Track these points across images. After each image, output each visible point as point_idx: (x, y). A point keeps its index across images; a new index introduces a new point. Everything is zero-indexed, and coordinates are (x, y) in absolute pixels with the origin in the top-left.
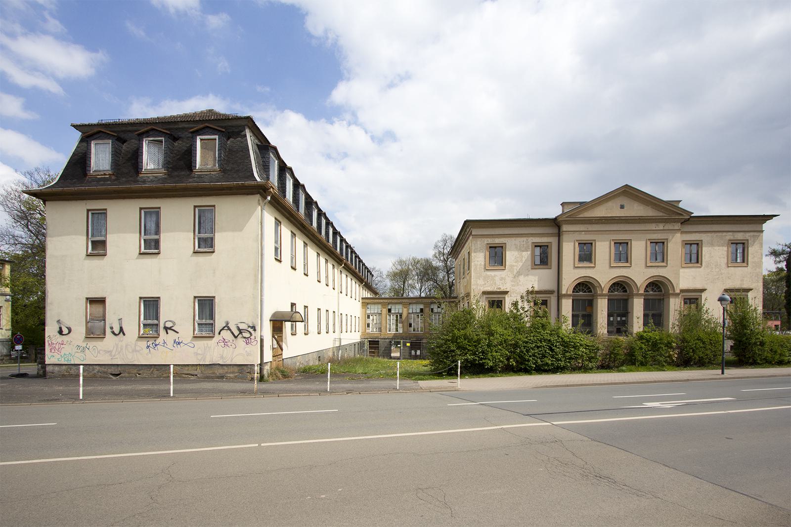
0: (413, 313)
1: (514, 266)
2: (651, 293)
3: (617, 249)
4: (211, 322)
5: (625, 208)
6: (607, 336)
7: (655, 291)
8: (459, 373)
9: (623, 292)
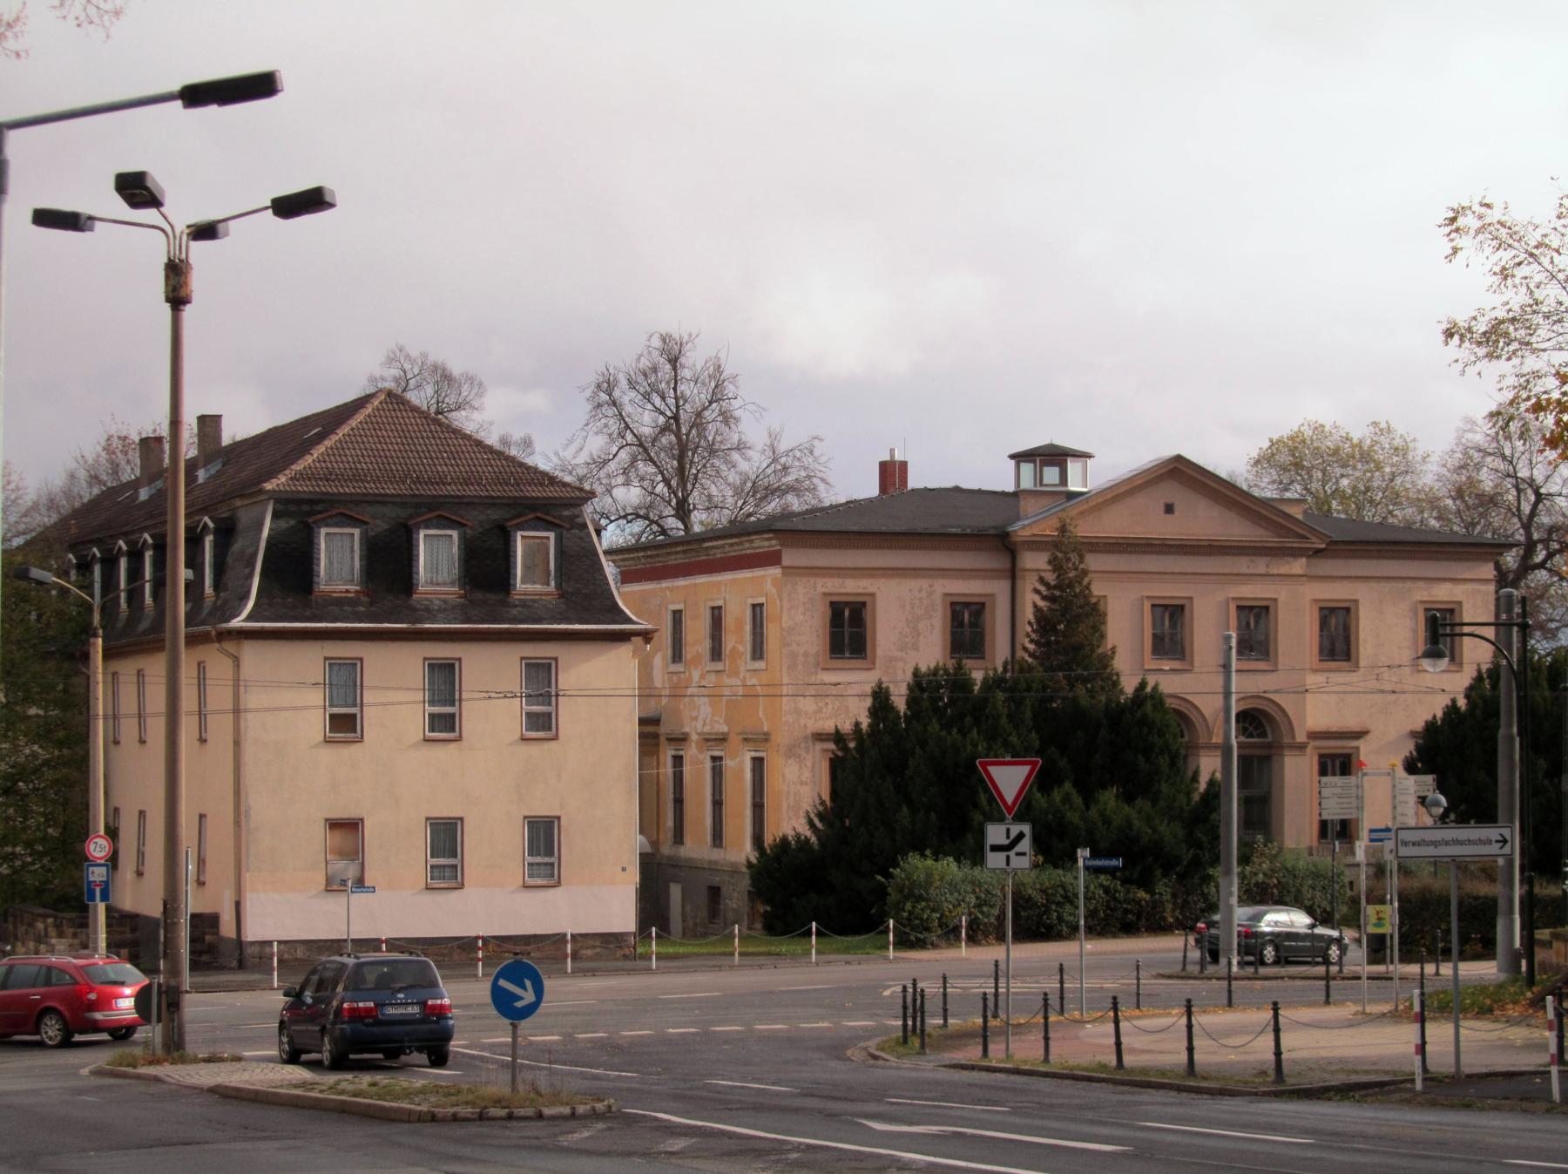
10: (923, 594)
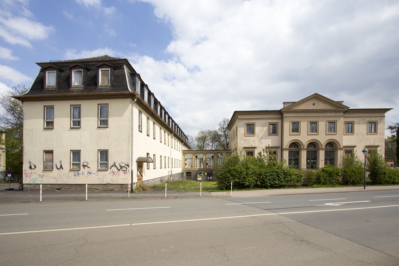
0: (208, 158)
1: (259, 134)
2: (329, 148)
3: (311, 126)
4: (107, 162)
5: (315, 105)
6: (306, 170)
7: (331, 147)
8: (231, 188)
9: (314, 147)
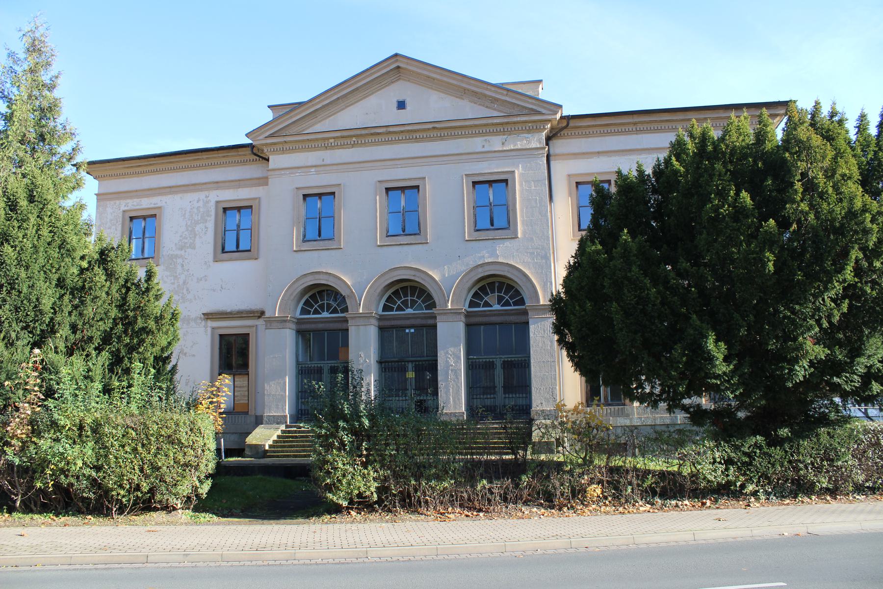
1: (177, 256)
2: (497, 307)
7: (507, 304)
10: (201, 204)
